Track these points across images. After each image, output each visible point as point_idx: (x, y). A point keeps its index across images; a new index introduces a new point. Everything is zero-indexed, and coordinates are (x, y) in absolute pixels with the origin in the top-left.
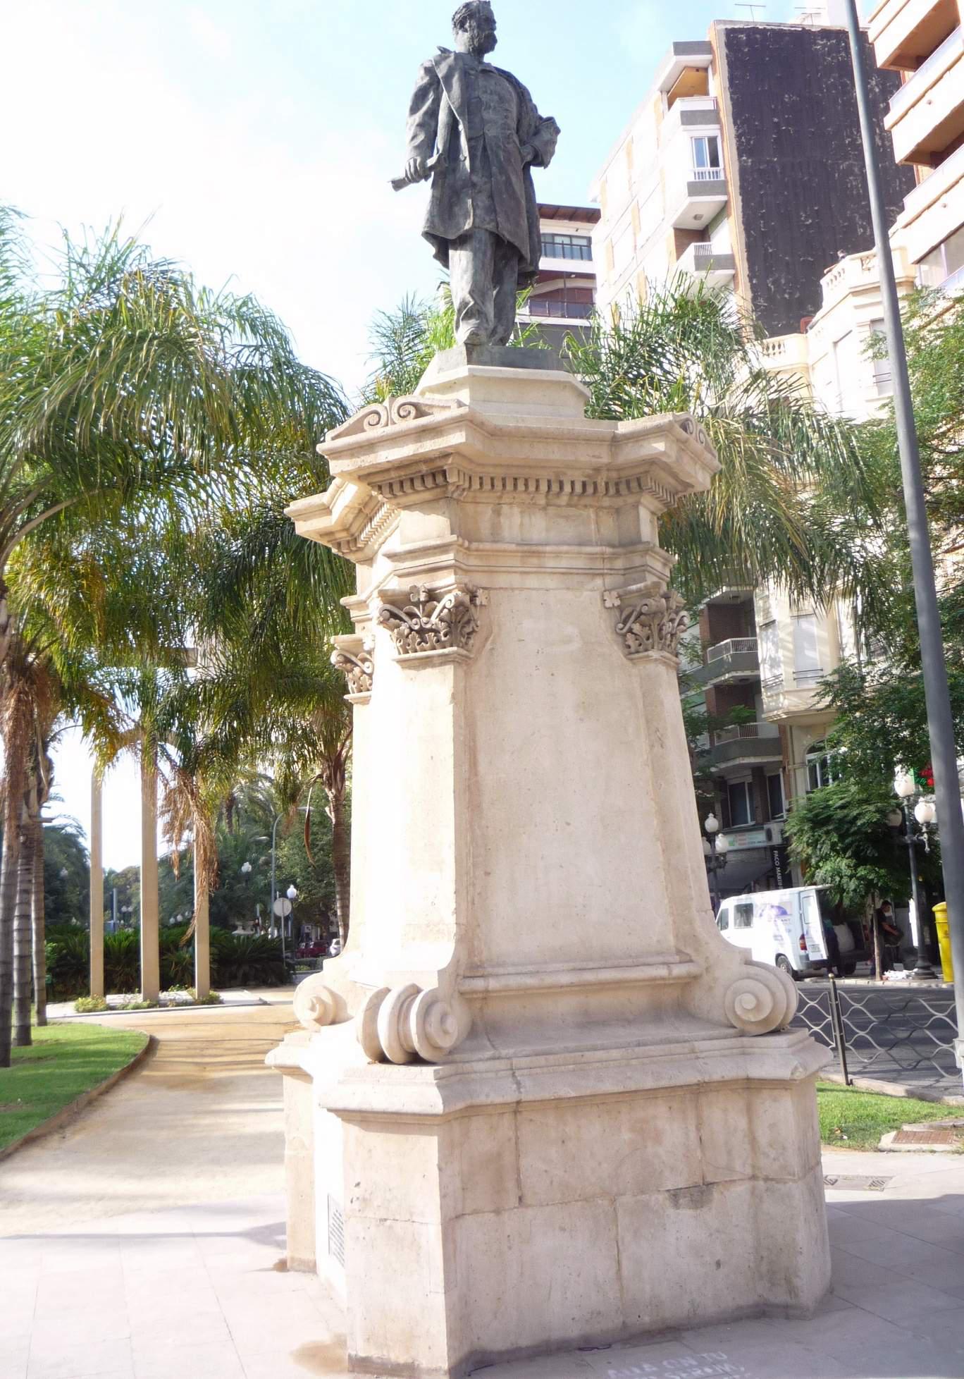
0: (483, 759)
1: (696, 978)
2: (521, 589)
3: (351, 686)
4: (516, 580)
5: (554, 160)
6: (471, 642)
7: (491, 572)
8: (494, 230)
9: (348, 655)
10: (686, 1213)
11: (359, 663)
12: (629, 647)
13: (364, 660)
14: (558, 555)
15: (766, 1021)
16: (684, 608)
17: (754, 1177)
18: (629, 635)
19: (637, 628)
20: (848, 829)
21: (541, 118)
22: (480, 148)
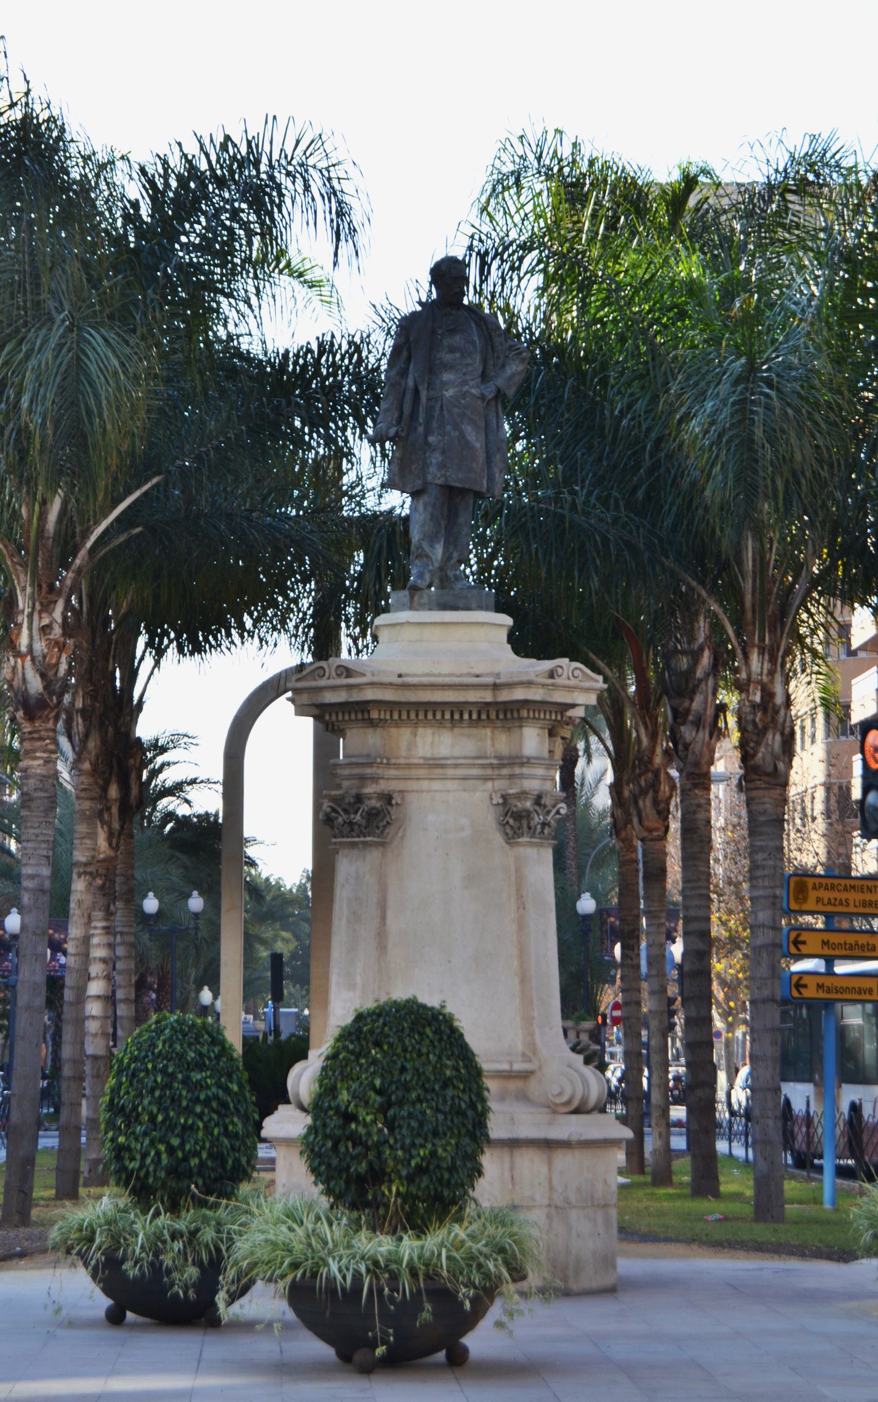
0: (390, 914)
1: (532, 1072)
2: (428, 791)
4: (425, 784)
7: (732, 526)
12: (507, 834)
14: (456, 766)
15: (568, 1103)
16: (562, 801)
17: (549, 1206)
19: (511, 821)
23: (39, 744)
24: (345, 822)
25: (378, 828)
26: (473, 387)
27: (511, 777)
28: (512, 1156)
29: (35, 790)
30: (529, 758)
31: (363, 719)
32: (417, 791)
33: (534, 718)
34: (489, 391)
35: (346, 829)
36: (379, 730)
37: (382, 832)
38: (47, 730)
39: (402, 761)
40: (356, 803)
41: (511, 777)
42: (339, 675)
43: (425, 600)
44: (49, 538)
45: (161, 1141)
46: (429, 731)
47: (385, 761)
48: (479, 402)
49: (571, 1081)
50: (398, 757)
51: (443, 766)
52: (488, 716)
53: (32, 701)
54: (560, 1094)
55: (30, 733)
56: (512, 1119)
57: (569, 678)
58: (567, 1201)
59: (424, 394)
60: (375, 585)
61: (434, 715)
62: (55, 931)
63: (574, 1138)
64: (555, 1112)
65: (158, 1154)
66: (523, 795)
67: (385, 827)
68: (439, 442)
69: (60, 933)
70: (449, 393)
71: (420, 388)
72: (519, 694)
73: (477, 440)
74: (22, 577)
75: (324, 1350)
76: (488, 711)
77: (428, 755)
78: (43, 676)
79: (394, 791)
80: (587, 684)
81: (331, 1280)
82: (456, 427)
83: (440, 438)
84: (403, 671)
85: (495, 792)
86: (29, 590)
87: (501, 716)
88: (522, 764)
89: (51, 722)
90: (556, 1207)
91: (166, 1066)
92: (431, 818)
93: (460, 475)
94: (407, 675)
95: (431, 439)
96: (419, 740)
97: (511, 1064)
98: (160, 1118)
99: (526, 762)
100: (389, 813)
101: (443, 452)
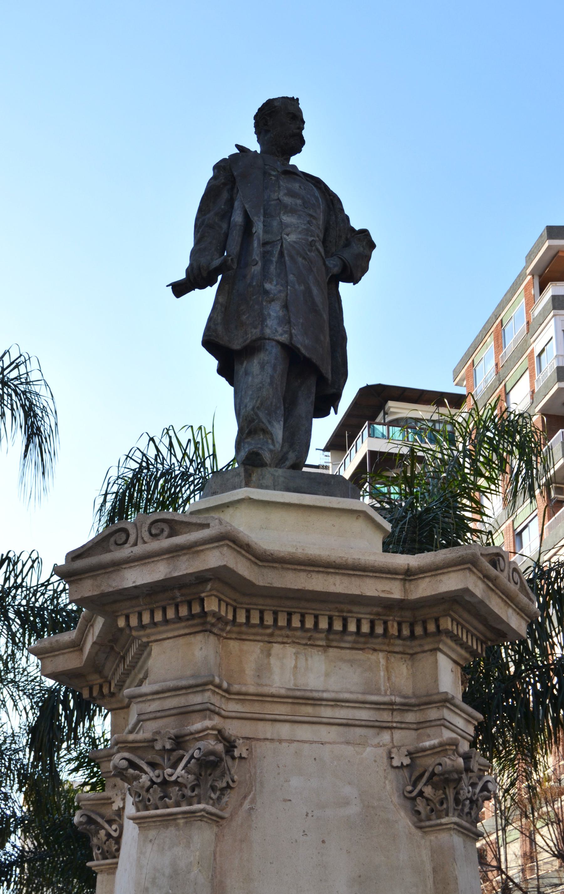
2: (292, 741)
3: (96, 852)
4: (285, 730)
5: (365, 278)
6: (225, 799)
8: (287, 342)
9: (94, 816)
11: (106, 826)
12: (418, 813)
13: (110, 822)
18: (419, 800)
19: (428, 791)
21: (353, 229)
22: (276, 253)
24: (153, 782)
25: (213, 789)
27: (420, 726)
31: (192, 616)
32: (272, 740)
35: (157, 792)
37: (219, 799)
41: (420, 726)
42: (154, 536)
46: (290, 650)
59: (258, 228)
60: (49, 733)
71: (255, 219)
76: (385, 623)
77: (291, 686)
92: (295, 782)
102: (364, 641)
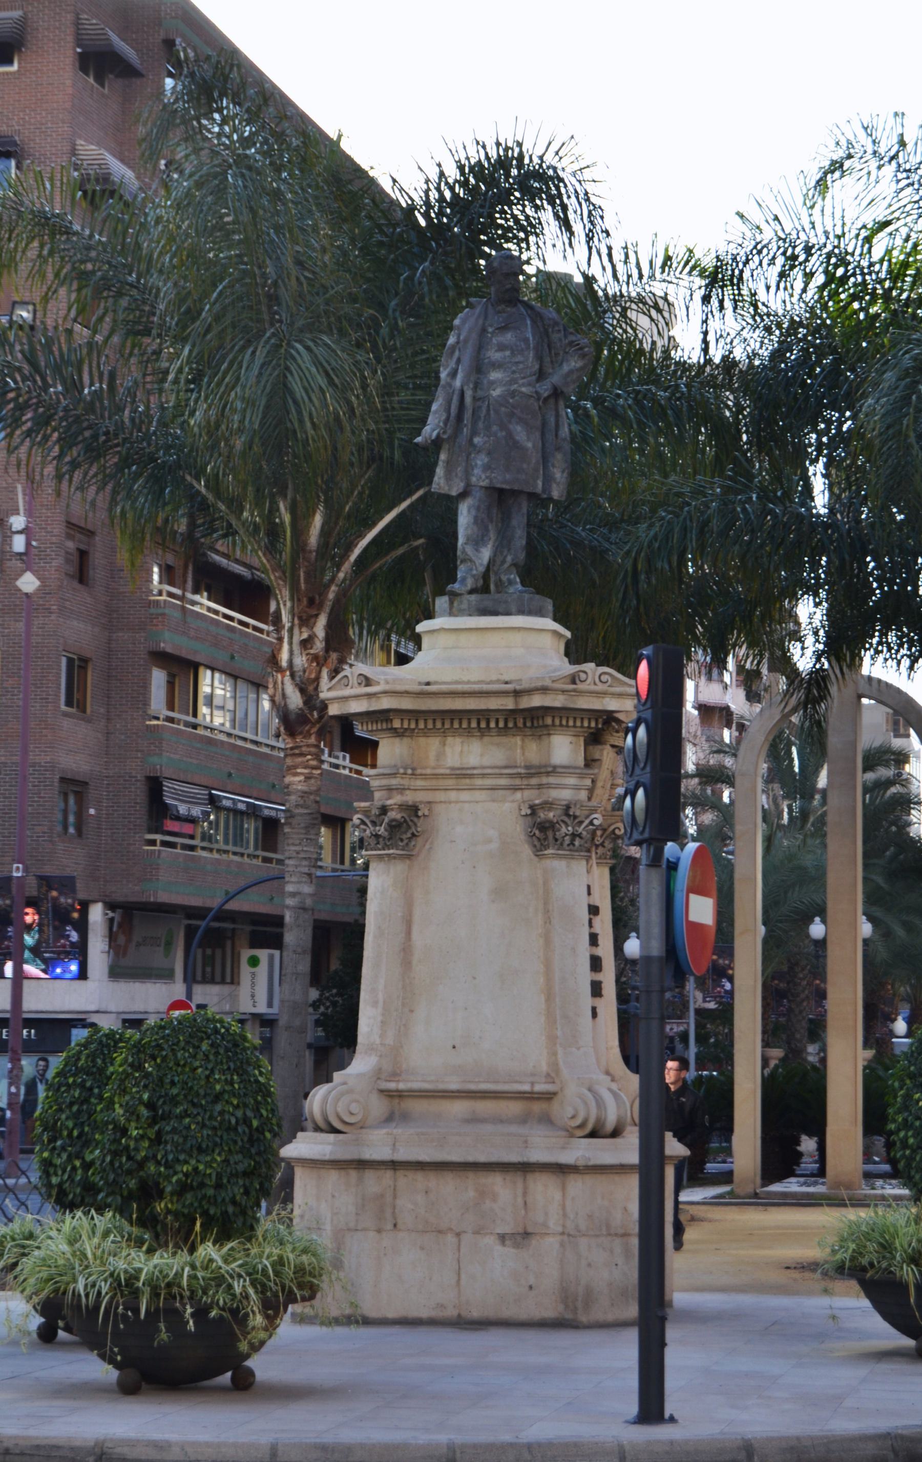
1: (555, 1094)
2: (457, 802)
4: (453, 795)
10: (509, 1251)
14: (484, 776)
15: (582, 1126)
17: (563, 1233)
19: (537, 832)
20: (387, 225)
23: (300, 759)
25: (402, 840)
26: (523, 385)
27: (540, 786)
28: (525, 1180)
29: (297, 806)
30: (555, 767)
33: (561, 725)
34: (545, 389)
36: (405, 740)
38: (308, 746)
39: (429, 771)
40: (380, 815)
43: (465, 606)
44: (310, 552)
45: (77, 1157)
46: (458, 740)
47: (409, 771)
48: (532, 401)
49: (586, 1103)
50: (425, 768)
51: (471, 776)
52: (515, 723)
53: (293, 717)
54: (573, 1117)
55: (292, 749)
56: (526, 1142)
57: (595, 684)
58: (577, 1228)
61: (460, 724)
62: (720, 957)
63: (581, 1163)
64: (572, 1136)
65: (74, 1169)
66: (548, 805)
67: (410, 839)
68: (485, 443)
69: (724, 959)
70: (496, 393)
72: (537, 701)
73: (529, 439)
74: (284, 590)
75: (107, 1373)
77: (457, 765)
78: (302, 691)
79: (421, 802)
80: (618, 689)
81: (76, 1295)
82: (503, 427)
83: (486, 439)
84: (431, 679)
85: (524, 802)
86: (289, 604)
87: (529, 724)
88: (548, 774)
89: (313, 737)
90: (569, 1235)
91: (84, 1081)
92: (459, 829)
93: (508, 476)
94: (436, 683)
95: (476, 440)
96: (448, 750)
97: (532, 1084)
98: (75, 1133)
99: (554, 770)
100: (415, 825)
101: (489, 453)
102: (504, 731)
